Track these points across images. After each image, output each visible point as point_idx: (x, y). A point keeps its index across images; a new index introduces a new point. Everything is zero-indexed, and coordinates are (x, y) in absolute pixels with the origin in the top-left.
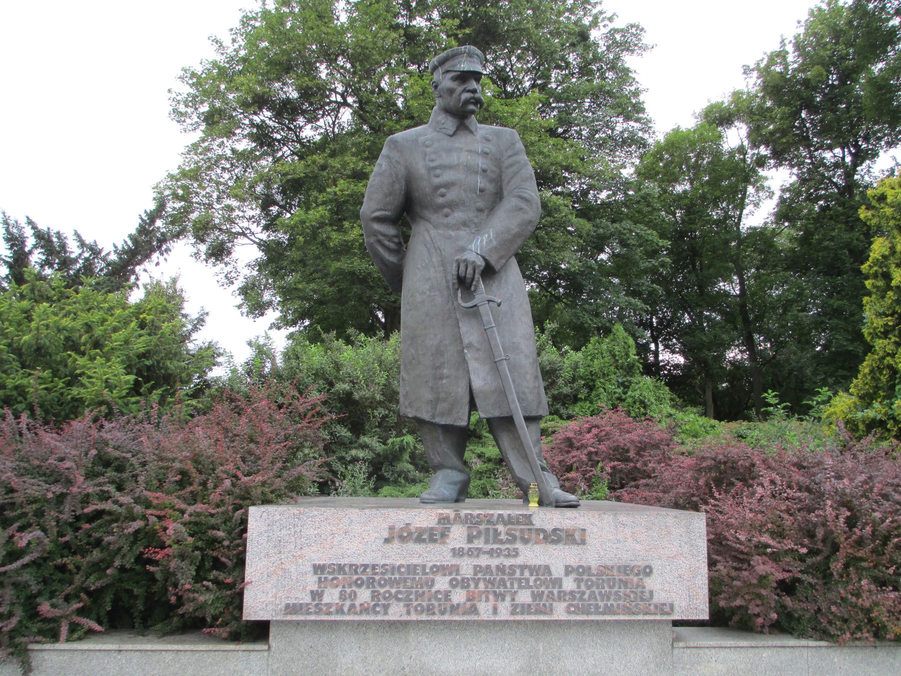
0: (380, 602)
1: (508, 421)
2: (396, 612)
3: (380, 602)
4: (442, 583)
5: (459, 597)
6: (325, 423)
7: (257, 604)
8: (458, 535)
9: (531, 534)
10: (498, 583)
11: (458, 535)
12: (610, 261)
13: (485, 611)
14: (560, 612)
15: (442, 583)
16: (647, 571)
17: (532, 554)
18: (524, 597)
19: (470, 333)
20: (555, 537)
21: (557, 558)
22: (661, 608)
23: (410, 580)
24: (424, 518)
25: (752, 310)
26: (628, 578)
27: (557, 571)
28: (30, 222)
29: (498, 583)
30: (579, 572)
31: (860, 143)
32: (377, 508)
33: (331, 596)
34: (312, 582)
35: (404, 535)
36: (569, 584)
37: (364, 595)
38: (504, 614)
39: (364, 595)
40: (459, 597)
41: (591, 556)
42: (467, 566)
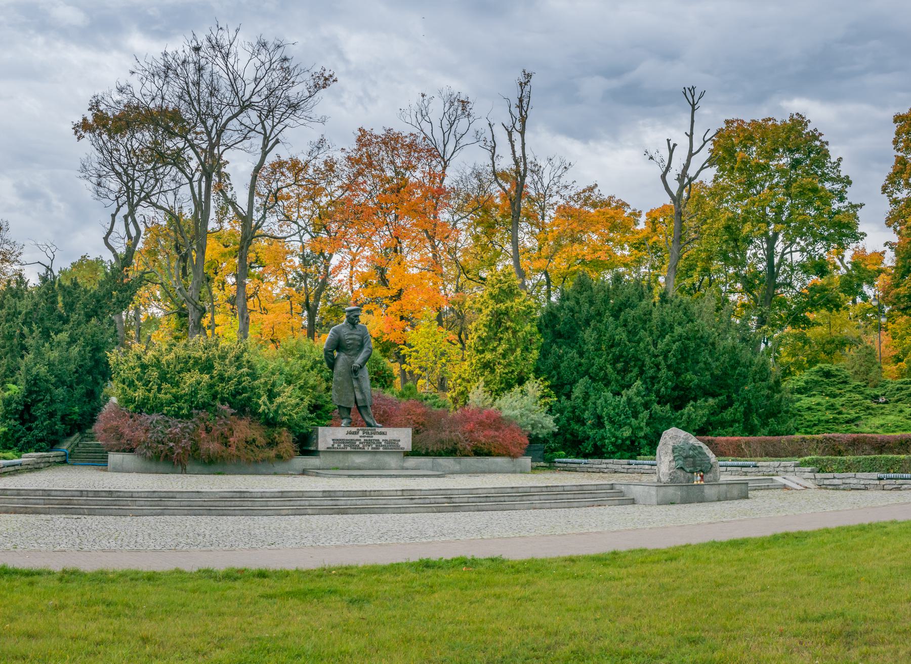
0: (345, 447)
1: (366, 407)
2: (349, 449)
4: (358, 443)
5: (361, 446)
6: (497, 429)
7: (321, 447)
8: (361, 433)
10: (369, 443)
11: (361, 433)
13: (366, 449)
14: (381, 449)
15: (358, 443)
17: (376, 437)
18: (374, 446)
19: (355, 383)
20: (383, 433)
21: (381, 438)
23: (351, 443)
24: (354, 429)
25: (188, 232)
26: (394, 443)
29: (369, 443)
30: (385, 441)
33: (336, 445)
34: (332, 442)
35: (383, 433)
37: (342, 445)
39: (342, 445)
40: (361, 446)
41: (387, 437)
42: (362, 440)
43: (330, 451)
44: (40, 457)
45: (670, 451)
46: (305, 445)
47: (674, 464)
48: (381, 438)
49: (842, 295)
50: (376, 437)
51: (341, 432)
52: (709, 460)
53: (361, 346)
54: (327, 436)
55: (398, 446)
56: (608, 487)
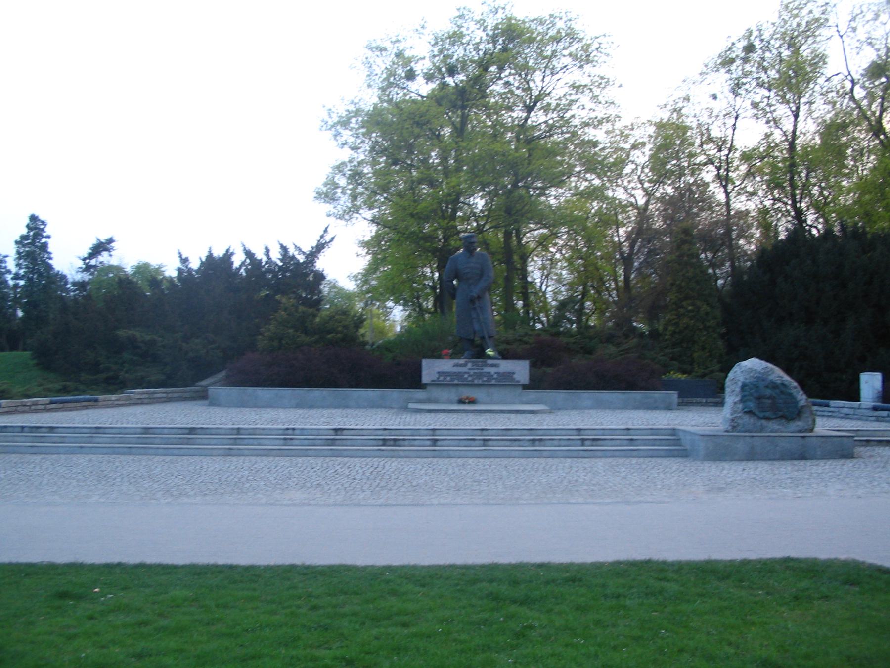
0: (452, 380)
2: (456, 382)
3: (452, 380)
4: (466, 376)
7: (425, 379)
8: (469, 365)
9: (487, 365)
10: (480, 375)
12: (395, 288)
13: (476, 382)
14: (493, 382)
16: (514, 373)
17: (487, 369)
18: (485, 379)
20: (493, 365)
21: (493, 370)
22: (518, 381)
23: (458, 375)
24: (462, 361)
27: (493, 373)
28: (333, 239)
31: (433, 154)
32: (299, 406)
34: (437, 376)
36: (495, 376)
38: (480, 382)
39: (449, 378)
43: (436, 384)
44: (144, 393)
45: (738, 390)
46: (410, 379)
47: (740, 406)
48: (493, 370)
49: (597, 182)
50: (487, 369)
51: (446, 365)
52: (797, 402)
53: (481, 276)
54: (430, 369)
55: (513, 379)
56: (439, 443)
